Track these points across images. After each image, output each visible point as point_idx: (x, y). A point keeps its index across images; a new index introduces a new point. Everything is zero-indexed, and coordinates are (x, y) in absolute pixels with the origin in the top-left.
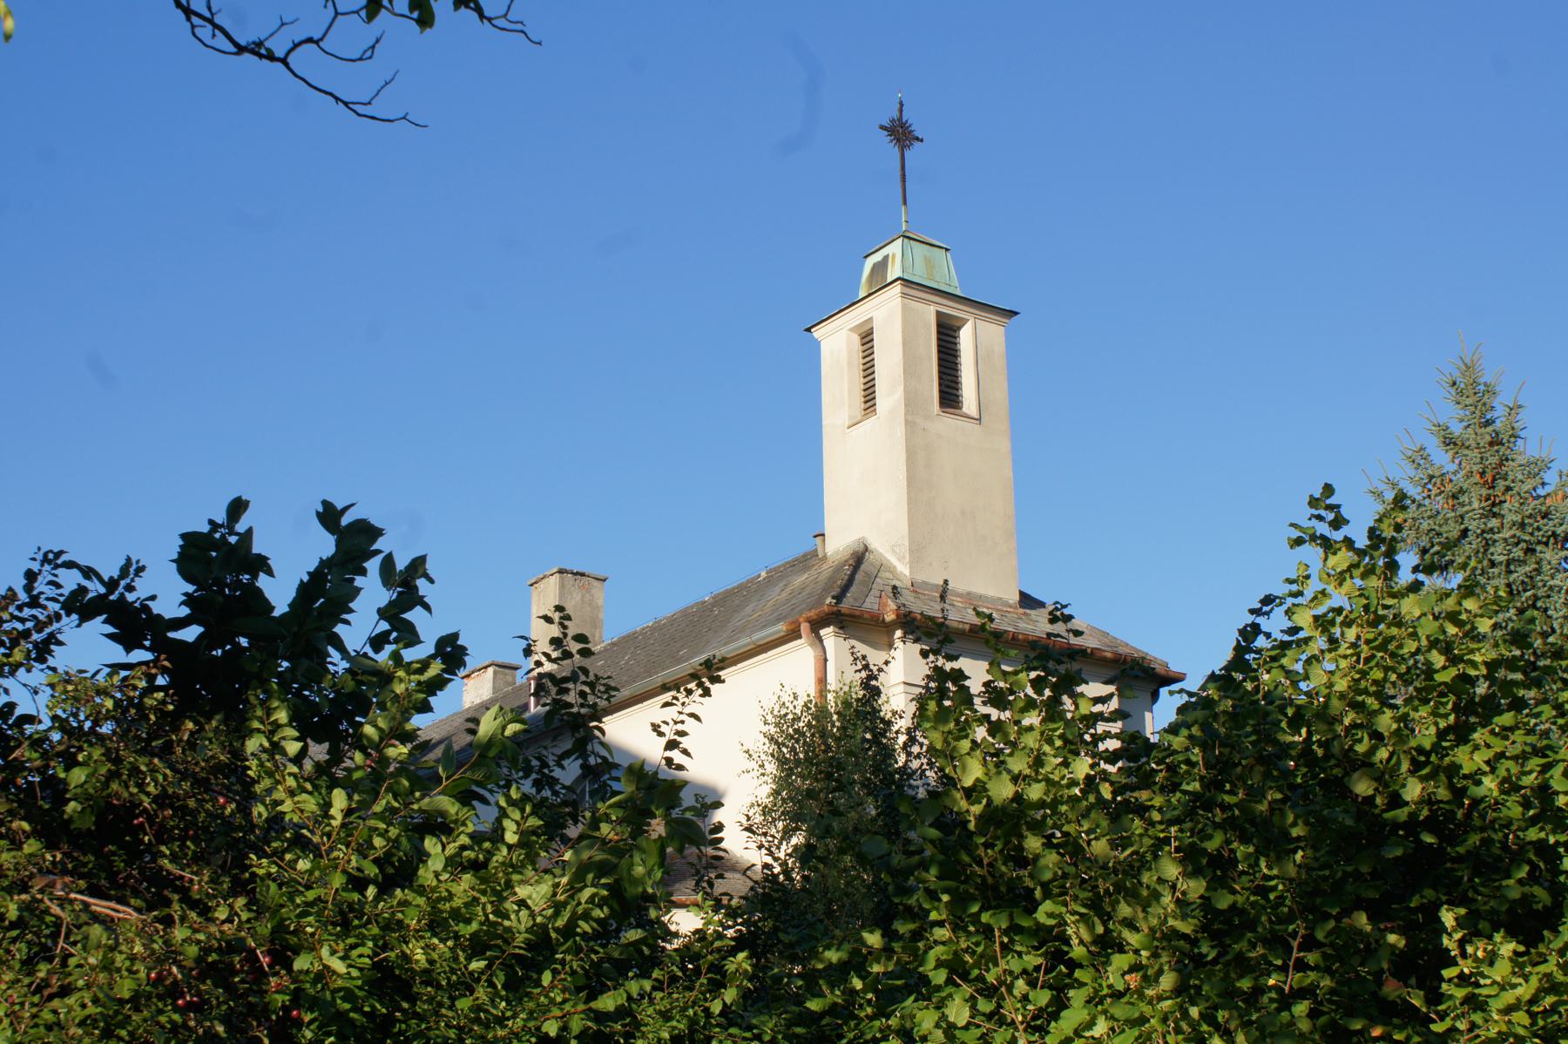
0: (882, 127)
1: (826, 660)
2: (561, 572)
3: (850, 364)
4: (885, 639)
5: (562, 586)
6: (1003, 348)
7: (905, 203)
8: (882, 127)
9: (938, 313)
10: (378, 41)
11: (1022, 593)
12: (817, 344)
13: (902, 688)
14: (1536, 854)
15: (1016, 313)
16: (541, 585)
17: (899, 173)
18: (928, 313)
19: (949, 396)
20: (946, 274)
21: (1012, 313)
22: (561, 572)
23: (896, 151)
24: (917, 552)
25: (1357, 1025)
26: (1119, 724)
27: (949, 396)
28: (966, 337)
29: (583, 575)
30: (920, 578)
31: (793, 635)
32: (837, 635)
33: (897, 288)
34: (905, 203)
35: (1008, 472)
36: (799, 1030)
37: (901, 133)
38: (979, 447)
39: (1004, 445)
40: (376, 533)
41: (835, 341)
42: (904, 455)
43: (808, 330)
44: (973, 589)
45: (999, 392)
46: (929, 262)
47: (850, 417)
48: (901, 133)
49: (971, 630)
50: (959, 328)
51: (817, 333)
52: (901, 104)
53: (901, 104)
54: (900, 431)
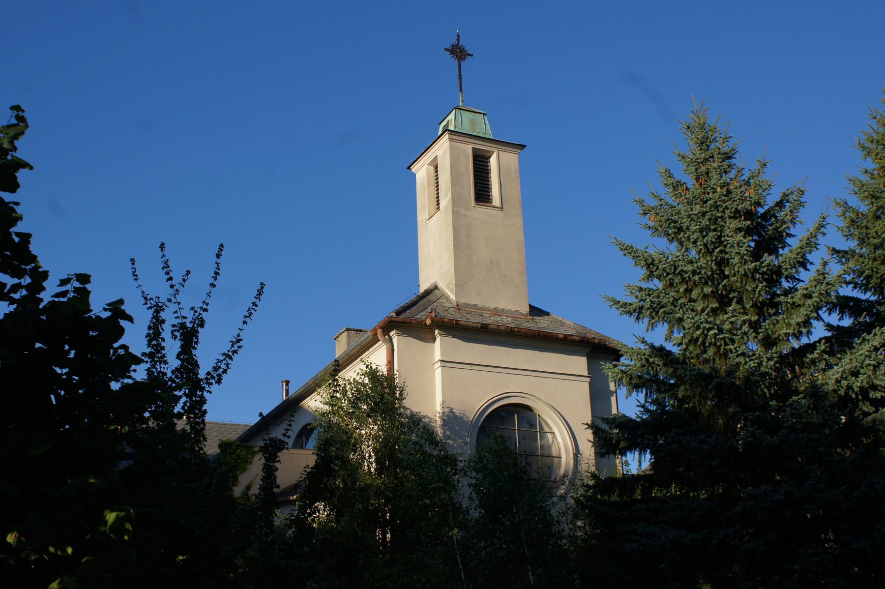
0: (446, 50)
1: (393, 350)
2: (348, 330)
3: (429, 184)
5: (349, 338)
6: (517, 166)
7: (461, 91)
8: (446, 50)
9: (473, 148)
11: (530, 306)
12: (414, 175)
13: (439, 364)
15: (525, 146)
16: (339, 338)
17: (458, 74)
18: (467, 149)
19: (482, 194)
20: (483, 127)
21: (522, 147)
22: (348, 330)
23: (456, 62)
25: (112, 428)
27: (482, 194)
28: (493, 161)
29: (361, 331)
30: (462, 301)
32: (398, 335)
33: (446, 136)
34: (461, 91)
35: (521, 237)
37: (459, 52)
38: (502, 226)
40: (89, 282)
41: (422, 171)
42: (452, 231)
43: (409, 168)
44: (498, 306)
45: (515, 192)
47: (429, 214)
48: (459, 52)
49: (482, 327)
50: (490, 157)
52: (459, 36)
53: (459, 36)
54: (450, 217)
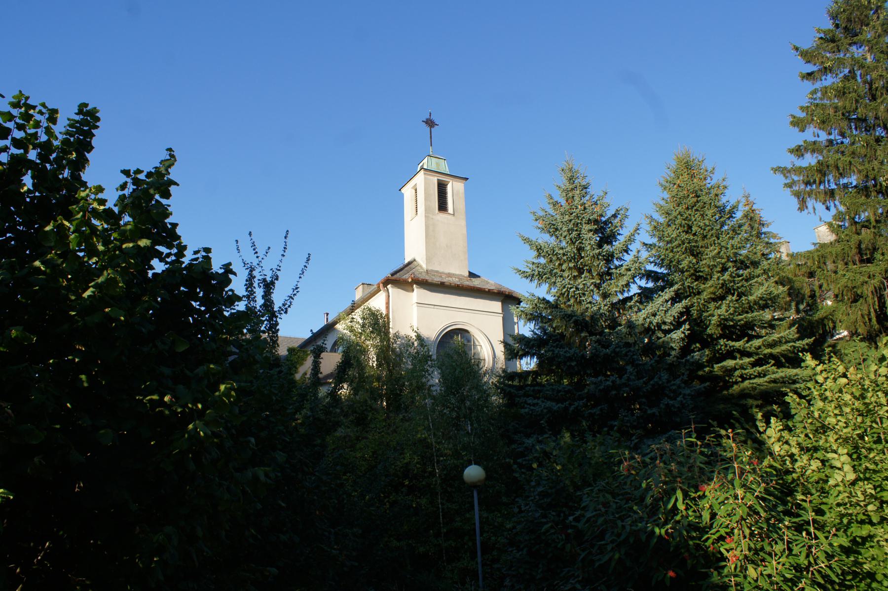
4: (410, 288)
10: (308, 260)
12: (403, 195)
14: (691, 442)
19: (442, 206)
20: (444, 167)
24: (429, 260)
26: (228, 349)
27: (442, 206)
30: (430, 268)
31: (378, 290)
35: (464, 231)
36: (28, 181)
37: (430, 123)
38: (453, 225)
39: (463, 223)
41: (408, 191)
45: (461, 205)
46: (438, 164)
48: (430, 123)
51: (403, 191)
